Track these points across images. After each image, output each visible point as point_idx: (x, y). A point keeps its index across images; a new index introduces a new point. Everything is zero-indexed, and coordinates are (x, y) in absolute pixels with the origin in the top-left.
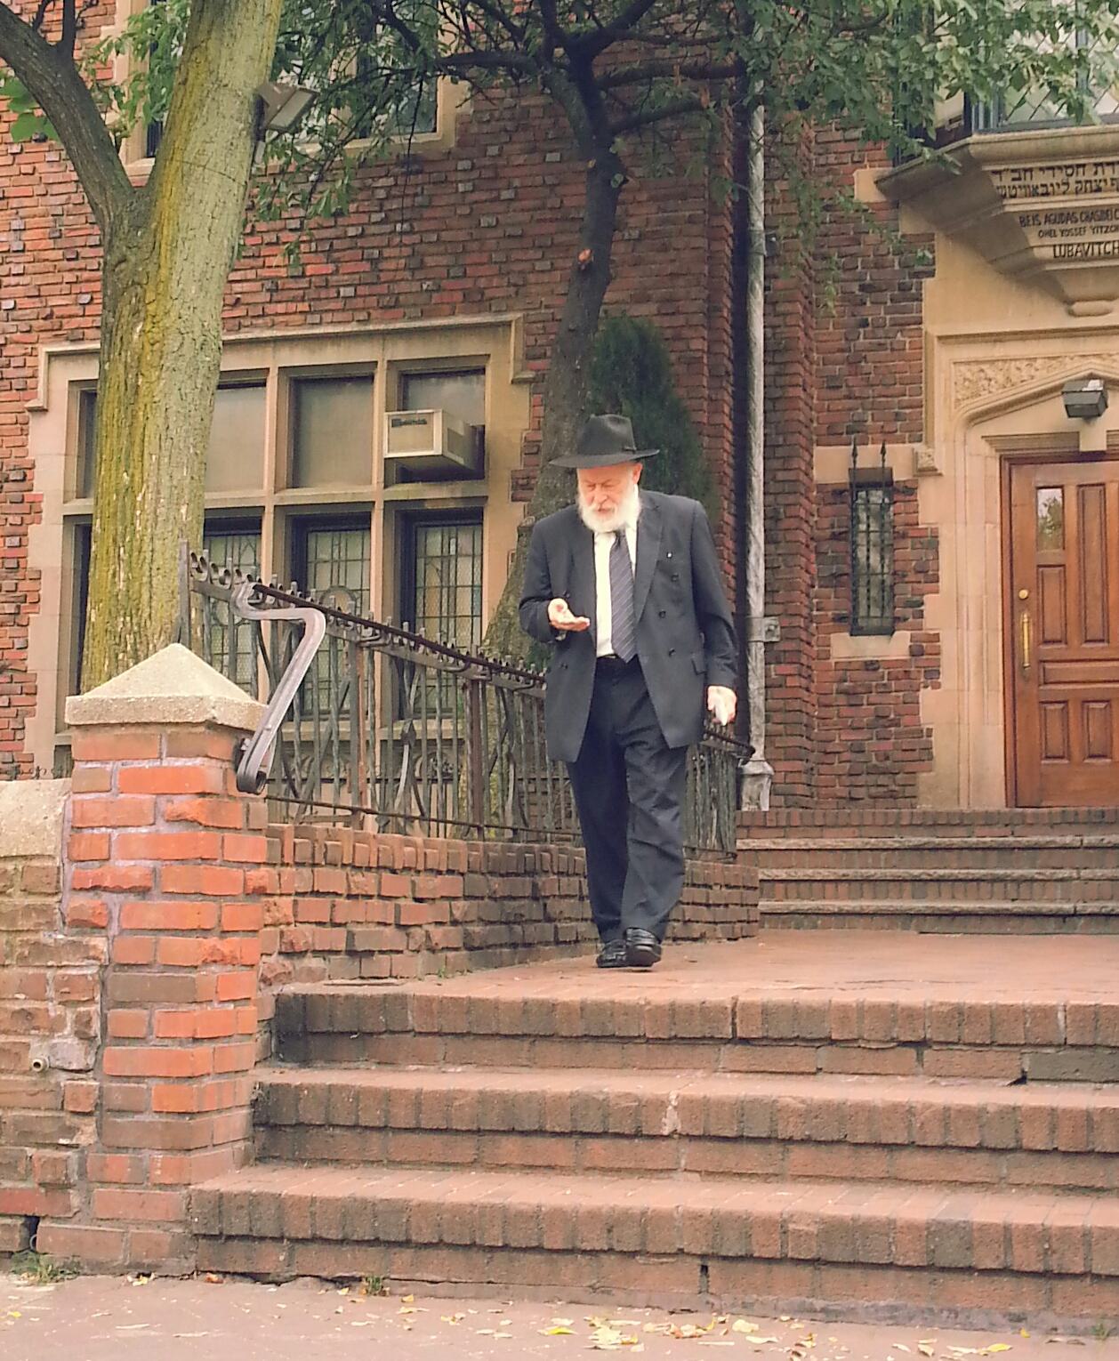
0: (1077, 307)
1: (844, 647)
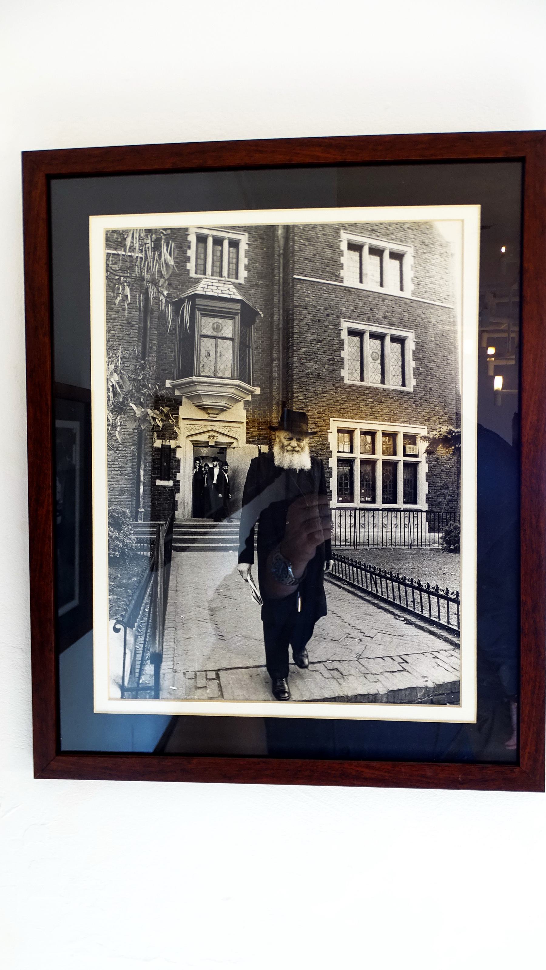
0: (210, 415)
1: (159, 483)
